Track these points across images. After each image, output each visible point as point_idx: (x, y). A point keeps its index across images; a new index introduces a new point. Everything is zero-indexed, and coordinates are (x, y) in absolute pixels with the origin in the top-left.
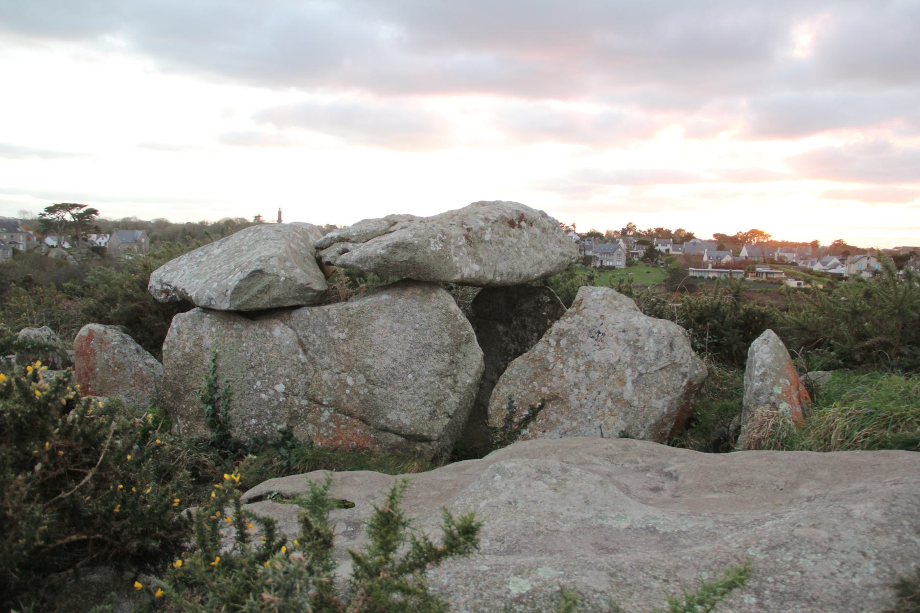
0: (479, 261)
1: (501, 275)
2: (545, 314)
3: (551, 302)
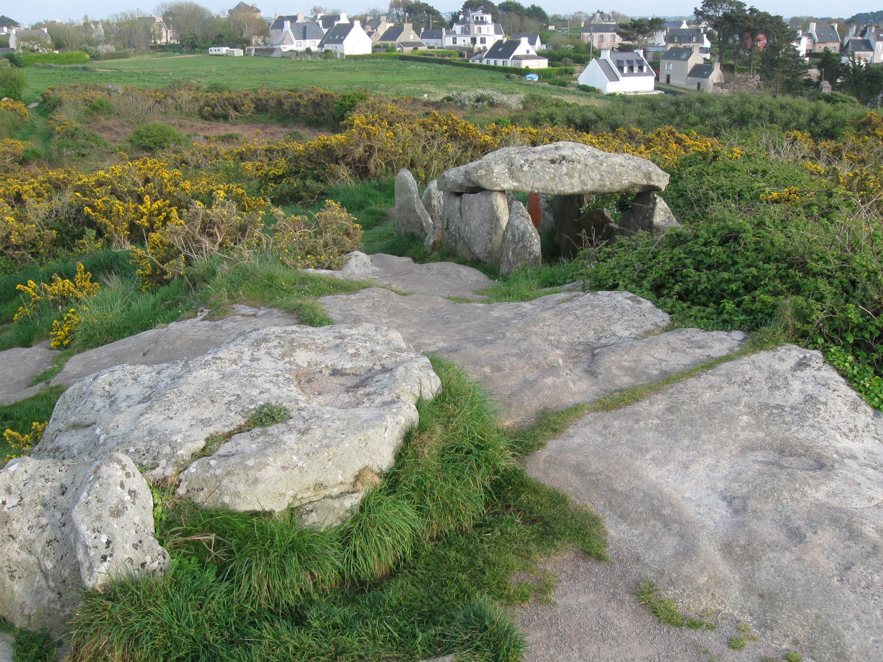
0: (518, 181)
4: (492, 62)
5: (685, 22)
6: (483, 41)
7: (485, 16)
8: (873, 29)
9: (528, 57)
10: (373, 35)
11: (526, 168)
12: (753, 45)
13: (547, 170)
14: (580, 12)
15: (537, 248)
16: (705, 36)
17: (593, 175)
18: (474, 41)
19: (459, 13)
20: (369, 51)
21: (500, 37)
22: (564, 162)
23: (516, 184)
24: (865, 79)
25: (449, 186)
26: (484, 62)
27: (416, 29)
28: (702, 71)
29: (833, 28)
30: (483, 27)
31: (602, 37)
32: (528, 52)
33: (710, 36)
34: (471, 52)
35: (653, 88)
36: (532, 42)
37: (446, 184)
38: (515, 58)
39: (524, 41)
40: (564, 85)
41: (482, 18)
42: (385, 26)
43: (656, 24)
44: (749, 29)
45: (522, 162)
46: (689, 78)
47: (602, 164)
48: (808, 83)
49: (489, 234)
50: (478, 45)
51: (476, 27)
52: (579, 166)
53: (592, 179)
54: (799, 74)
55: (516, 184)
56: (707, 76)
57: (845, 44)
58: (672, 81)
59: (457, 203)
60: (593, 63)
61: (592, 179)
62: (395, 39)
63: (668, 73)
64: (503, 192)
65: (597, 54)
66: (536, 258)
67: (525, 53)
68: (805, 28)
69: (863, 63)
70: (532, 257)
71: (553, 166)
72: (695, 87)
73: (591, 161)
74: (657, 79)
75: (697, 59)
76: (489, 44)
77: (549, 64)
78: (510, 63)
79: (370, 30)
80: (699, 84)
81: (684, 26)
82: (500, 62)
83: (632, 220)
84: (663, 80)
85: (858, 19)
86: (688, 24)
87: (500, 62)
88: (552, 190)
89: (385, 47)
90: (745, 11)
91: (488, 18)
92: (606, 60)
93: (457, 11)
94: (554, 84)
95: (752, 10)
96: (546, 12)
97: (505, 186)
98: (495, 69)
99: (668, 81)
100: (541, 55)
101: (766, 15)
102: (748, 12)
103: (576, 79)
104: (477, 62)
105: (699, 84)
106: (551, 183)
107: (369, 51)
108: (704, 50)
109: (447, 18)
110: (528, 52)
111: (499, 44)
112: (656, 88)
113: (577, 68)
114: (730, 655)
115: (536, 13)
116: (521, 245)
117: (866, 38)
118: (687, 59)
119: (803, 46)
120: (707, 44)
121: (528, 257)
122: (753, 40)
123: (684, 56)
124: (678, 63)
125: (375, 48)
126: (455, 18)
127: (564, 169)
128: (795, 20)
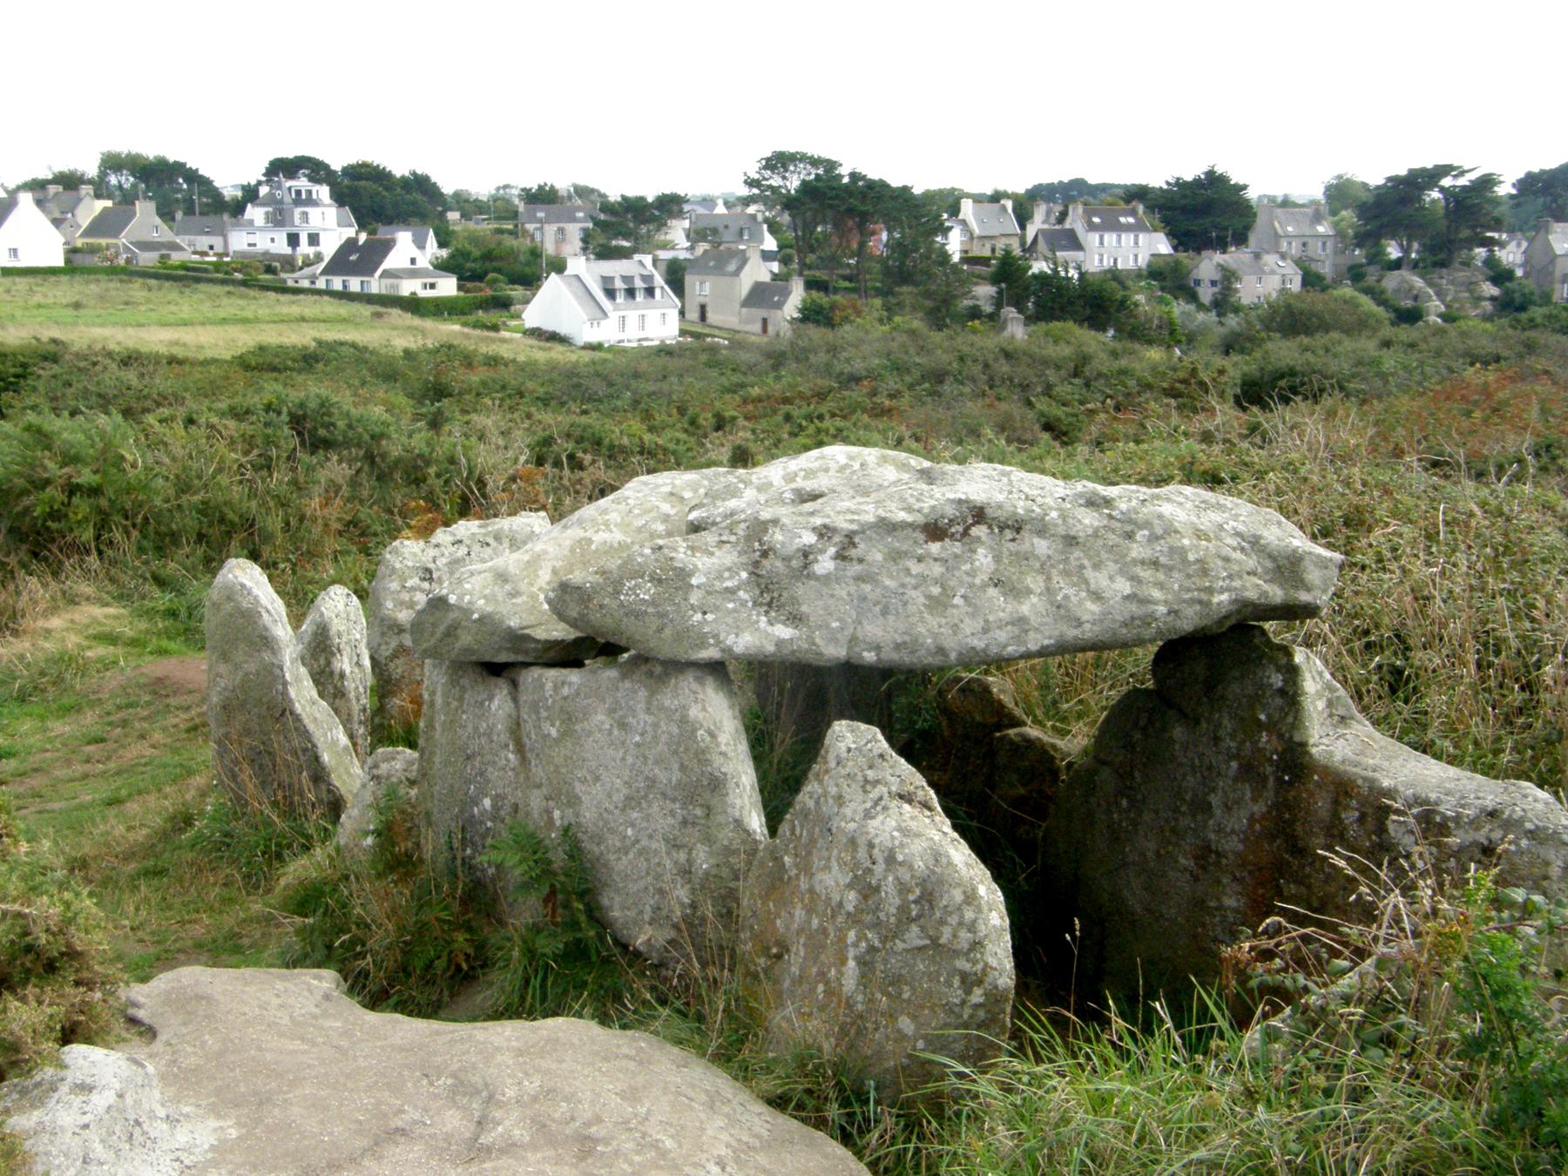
0: (795, 619)
1: (878, 648)
2: (1263, 717)
3: (1282, 692)
4: (337, 283)
5: (720, 202)
6: (314, 239)
7: (315, 188)
8: (1080, 209)
9: (413, 274)
10: (66, 225)
11: (825, 564)
12: (862, 245)
13: (916, 568)
14: (506, 187)
15: (1000, 957)
16: (765, 227)
17: (1099, 579)
18: (293, 240)
19: (260, 183)
20: (59, 261)
21: (350, 232)
22: (979, 531)
23: (784, 632)
24: (1081, 302)
25: (465, 639)
26: (321, 284)
27: (166, 213)
28: (761, 296)
29: (1004, 208)
30: (313, 212)
31: (561, 230)
32: (413, 261)
33: (774, 229)
34: (289, 263)
35: (677, 332)
36: (420, 244)
37: (451, 632)
38: (387, 274)
39: (404, 238)
40: (495, 328)
41: (309, 192)
42: (92, 208)
43: (670, 205)
44: (851, 211)
45: (809, 538)
46: (744, 310)
47: (1130, 536)
48: (975, 313)
49: (676, 846)
50: (304, 248)
51: (298, 211)
52: (1042, 546)
53: (1097, 596)
54: (955, 297)
55: (784, 632)
56: (779, 306)
57: (1029, 240)
58: (712, 317)
59: (499, 703)
60: (553, 285)
61: (1097, 596)
62: (116, 235)
63: (702, 300)
64: (716, 669)
65: (559, 267)
66: (994, 997)
67: (407, 265)
68: (955, 210)
69: (1073, 274)
70: (977, 996)
71: (935, 548)
72: (757, 327)
73: (1088, 520)
74: (682, 313)
75: (759, 271)
76: (329, 247)
77: (460, 288)
78: (375, 286)
79: (57, 215)
80: (765, 322)
81: (720, 209)
82: (355, 284)
83: (1178, 732)
84: (693, 315)
85: (1039, 194)
86: (726, 204)
87: (355, 284)
88: (941, 650)
89: (93, 250)
90: (842, 177)
91: (323, 192)
92: (577, 277)
93: (253, 182)
94: (475, 327)
95: (854, 176)
96: (440, 184)
97: (744, 642)
98: (345, 296)
99: (703, 317)
100: (443, 267)
101: (883, 185)
102: (846, 180)
103: (518, 316)
104: (305, 284)
105: (765, 322)
106: (933, 621)
107: (59, 261)
108: (767, 256)
109: (230, 191)
110: (413, 261)
111: (350, 245)
112: (683, 333)
113: (517, 292)
114: (4, 525)
115: (421, 185)
116: (914, 937)
117: (1067, 225)
118: (737, 273)
119: (954, 244)
120: (770, 243)
121: (956, 995)
122: (862, 234)
123: (732, 267)
124: (722, 281)
125: (72, 252)
126: (250, 194)
127: (983, 558)
128: (930, 196)
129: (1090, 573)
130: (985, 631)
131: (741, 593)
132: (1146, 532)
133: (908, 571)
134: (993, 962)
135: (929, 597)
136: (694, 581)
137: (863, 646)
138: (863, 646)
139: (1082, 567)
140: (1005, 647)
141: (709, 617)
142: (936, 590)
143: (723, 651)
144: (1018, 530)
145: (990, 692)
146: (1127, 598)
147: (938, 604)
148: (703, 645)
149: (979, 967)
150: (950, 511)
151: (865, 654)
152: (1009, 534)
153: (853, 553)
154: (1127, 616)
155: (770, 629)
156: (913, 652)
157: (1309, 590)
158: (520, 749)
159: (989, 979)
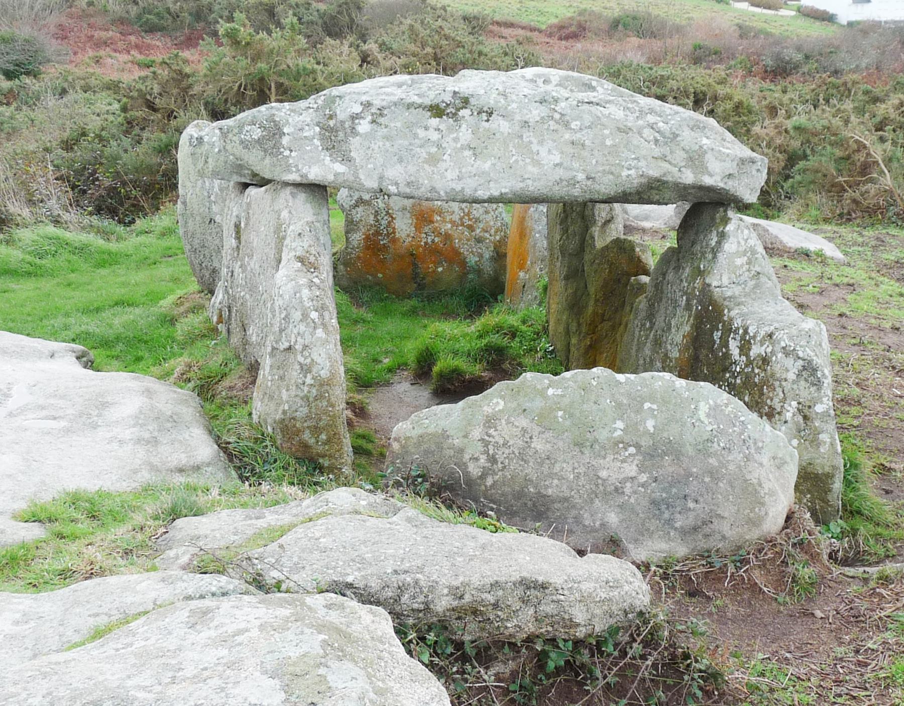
0: (346, 159)
13: (421, 133)
71: (435, 122)
129: (535, 147)
130: (460, 178)
131: (315, 141)
132: (578, 123)
133: (416, 136)
134: (319, 360)
135: (429, 154)
136: (286, 130)
137: (389, 182)
138: (389, 182)
139: (531, 142)
140: (476, 190)
141: (293, 154)
142: (434, 150)
143: (302, 176)
144: (490, 114)
145: (634, 250)
146: (556, 165)
147: (433, 160)
148: (288, 170)
149: (309, 361)
150: (448, 98)
151: (390, 187)
152: (484, 116)
153: (381, 120)
154: (557, 178)
155: (331, 165)
156: (418, 188)
157: (711, 175)
158: (238, 238)
159: (314, 370)
